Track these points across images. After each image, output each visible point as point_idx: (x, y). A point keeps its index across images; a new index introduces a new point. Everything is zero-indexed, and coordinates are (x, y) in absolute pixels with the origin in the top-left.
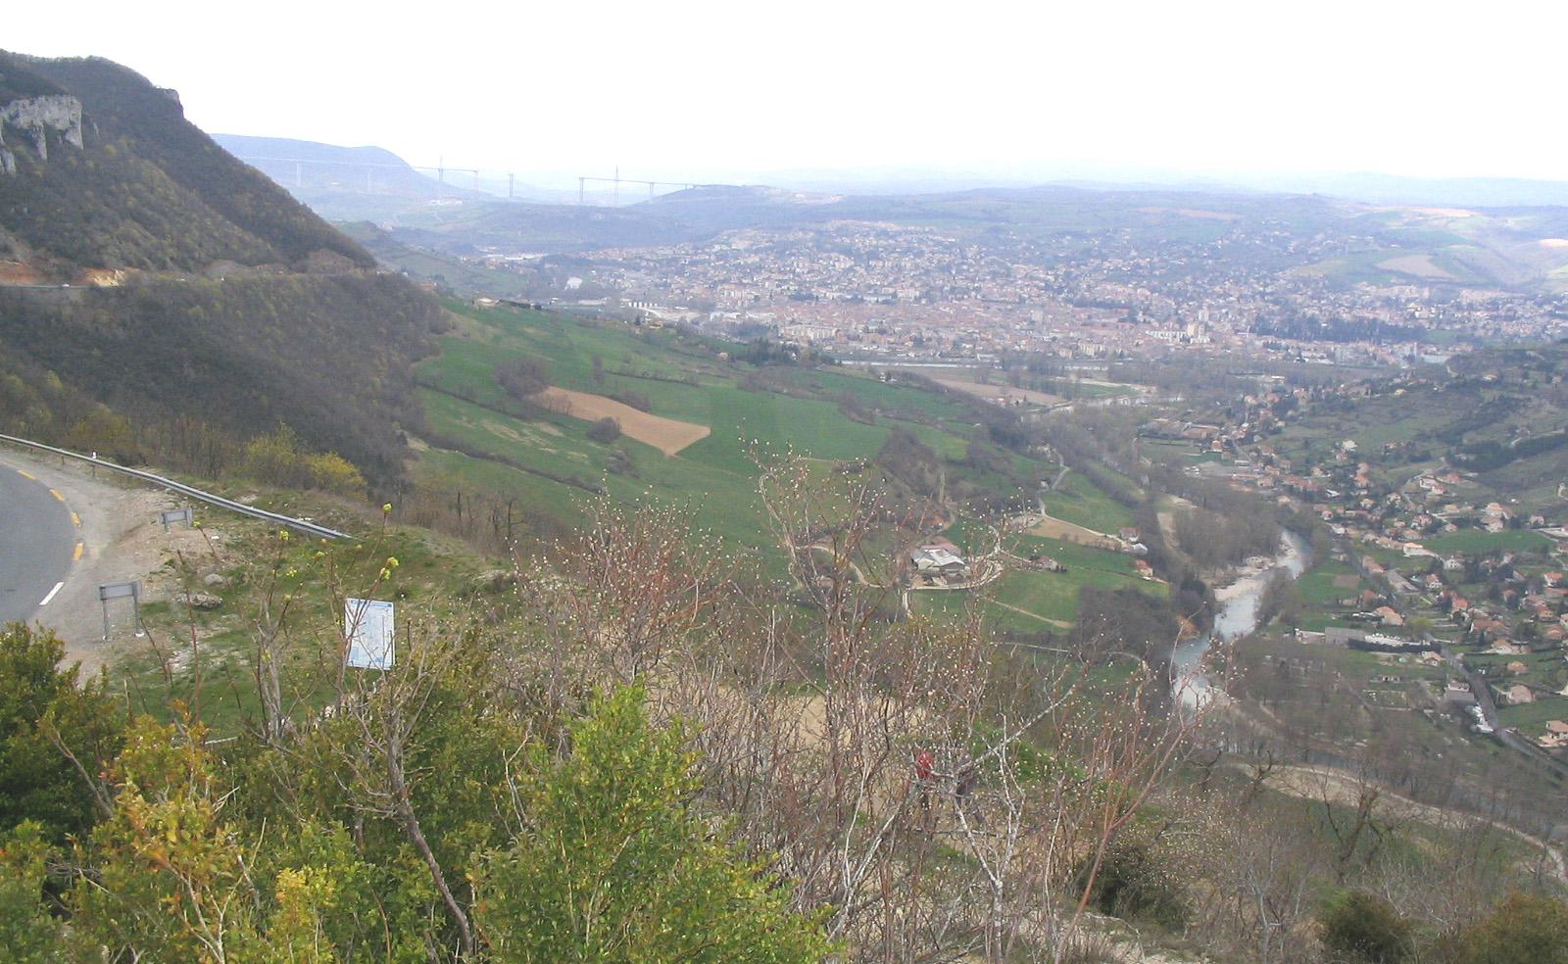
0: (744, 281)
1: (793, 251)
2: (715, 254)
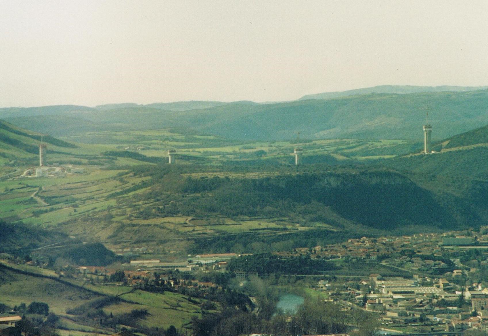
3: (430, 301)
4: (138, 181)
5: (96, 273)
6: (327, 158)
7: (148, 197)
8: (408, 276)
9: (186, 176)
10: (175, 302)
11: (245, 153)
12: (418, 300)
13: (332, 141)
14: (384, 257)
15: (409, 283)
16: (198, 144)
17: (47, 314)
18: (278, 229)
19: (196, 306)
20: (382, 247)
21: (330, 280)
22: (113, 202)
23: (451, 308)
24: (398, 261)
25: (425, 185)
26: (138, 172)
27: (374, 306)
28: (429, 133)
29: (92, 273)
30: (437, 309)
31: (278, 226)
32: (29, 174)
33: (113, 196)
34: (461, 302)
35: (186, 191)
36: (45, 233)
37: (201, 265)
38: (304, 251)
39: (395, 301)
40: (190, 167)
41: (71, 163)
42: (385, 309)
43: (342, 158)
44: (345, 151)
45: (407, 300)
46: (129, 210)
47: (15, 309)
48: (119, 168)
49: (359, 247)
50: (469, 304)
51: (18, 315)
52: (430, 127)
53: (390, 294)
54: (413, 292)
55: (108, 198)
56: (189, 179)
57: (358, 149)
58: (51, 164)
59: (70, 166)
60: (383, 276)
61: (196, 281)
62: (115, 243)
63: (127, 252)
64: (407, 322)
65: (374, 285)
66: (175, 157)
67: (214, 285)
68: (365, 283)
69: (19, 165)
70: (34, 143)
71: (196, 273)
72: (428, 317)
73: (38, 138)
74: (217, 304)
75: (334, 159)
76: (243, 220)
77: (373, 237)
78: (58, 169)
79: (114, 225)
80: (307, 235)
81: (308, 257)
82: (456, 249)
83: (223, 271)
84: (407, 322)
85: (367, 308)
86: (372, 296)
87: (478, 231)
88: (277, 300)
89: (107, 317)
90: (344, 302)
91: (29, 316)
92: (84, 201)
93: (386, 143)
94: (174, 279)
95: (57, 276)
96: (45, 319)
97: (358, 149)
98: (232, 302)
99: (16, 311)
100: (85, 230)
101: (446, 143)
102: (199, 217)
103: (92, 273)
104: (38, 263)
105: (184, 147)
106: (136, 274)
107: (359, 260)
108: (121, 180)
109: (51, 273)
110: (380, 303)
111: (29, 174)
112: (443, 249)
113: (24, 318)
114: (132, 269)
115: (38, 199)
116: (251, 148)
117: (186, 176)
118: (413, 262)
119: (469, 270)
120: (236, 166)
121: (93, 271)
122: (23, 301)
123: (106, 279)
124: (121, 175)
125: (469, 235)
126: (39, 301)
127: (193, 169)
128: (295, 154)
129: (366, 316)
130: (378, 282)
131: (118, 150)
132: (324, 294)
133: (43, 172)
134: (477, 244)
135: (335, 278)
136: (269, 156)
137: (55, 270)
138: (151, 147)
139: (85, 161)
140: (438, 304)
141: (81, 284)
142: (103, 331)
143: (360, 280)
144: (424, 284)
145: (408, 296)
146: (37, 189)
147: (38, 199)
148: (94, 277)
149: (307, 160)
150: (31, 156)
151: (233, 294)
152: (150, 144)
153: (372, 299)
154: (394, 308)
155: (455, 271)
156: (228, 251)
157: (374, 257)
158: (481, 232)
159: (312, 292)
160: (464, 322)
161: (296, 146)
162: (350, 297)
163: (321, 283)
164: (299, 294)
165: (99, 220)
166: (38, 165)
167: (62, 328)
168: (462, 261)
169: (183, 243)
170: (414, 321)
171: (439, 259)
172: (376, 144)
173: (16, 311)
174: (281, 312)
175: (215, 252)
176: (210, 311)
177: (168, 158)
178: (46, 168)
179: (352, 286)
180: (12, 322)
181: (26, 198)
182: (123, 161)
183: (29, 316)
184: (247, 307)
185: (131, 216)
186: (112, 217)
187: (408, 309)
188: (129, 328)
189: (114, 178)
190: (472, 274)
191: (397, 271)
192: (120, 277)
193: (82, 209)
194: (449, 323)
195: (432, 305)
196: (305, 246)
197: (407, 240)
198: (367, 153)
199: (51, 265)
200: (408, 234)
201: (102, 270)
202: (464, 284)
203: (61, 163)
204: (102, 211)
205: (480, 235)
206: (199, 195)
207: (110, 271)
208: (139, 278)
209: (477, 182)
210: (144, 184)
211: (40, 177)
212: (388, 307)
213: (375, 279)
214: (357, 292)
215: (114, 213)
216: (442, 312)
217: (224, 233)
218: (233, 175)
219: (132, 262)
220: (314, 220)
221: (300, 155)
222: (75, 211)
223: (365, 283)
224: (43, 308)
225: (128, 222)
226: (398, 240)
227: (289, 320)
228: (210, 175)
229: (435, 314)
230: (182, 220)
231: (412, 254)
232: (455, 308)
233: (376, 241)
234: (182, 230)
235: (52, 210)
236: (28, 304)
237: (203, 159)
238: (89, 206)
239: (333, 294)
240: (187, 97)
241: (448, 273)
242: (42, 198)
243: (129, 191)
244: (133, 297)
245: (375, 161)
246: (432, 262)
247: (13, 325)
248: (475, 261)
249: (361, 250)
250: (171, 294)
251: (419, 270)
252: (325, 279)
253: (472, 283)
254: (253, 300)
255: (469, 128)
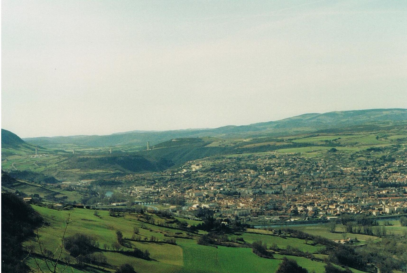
0: (200, 187)
1: (226, 170)
2: (184, 174)
3: (150, 192)
4: (64, 158)
5: (52, 186)
6: (120, 151)
7: (67, 163)
8: (143, 185)
9: (78, 157)
10: (75, 194)
11: (95, 150)
12: (146, 192)
13: (121, 146)
14: (137, 180)
15: (143, 187)
16: (82, 148)
17: (39, 197)
18: (105, 172)
19: (82, 195)
20: (136, 177)
21: (120, 187)
22: (57, 165)
23: (155, 194)
24: (140, 181)
25: (148, 159)
26: (64, 156)
27: (133, 194)
28: (149, 144)
29: (51, 186)
30: (151, 194)
31: (106, 172)
32: (33, 157)
33: (57, 163)
34: (158, 192)
35: (78, 162)
36: (38, 174)
37: (83, 183)
38: (113, 179)
39: (140, 193)
40: (79, 154)
41: (45, 153)
42: (137, 195)
43: (124, 151)
44: (125, 149)
45: (143, 192)
46: (61, 167)
47: (30, 196)
48: (58, 155)
49: (129, 177)
50: (160, 193)
51: (30, 197)
52: (149, 142)
53: (138, 191)
54: (145, 190)
55: (55, 164)
56: (79, 158)
57: (128, 149)
58: (39, 154)
59: (45, 155)
60: (136, 185)
61: (82, 188)
62: (58, 177)
63: (61, 179)
64: (143, 199)
65: (133, 188)
66: (75, 151)
67: (87, 189)
68: (131, 188)
69: (30, 154)
70: (34, 148)
71: (82, 185)
72: (149, 197)
73: (35, 146)
74: (87, 194)
75: (121, 152)
76: (96, 170)
77: (133, 175)
78: (41, 155)
79: (57, 172)
80: (114, 174)
81: (114, 181)
82: (157, 177)
83: (90, 185)
84: (143, 199)
85: (132, 195)
86: (133, 191)
87: (163, 172)
88: (106, 193)
89: (56, 198)
90: (125, 193)
91: (34, 198)
92: (49, 165)
93: (137, 147)
94: (75, 187)
95: (41, 186)
96: (38, 199)
97: (128, 149)
98: (92, 194)
99: (30, 196)
100: (49, 173)
101: (153, 147)
102: (82, 169)
103: (51, 186)
104: (36, 183)
105: (78, 149)
106: (64, 186)
107: (129, 181)
108: (59, 159)
109: (40, 186)
110: (135, 193)
111: (33, 157)
112: (153, 177)
113: (32, 198)
114: (63, 184)
115: (35, 164)
116: (97, 149)
117: (78, 157)
118: (145, 181)
119: (160, 183)
120: (93, 154)
121: (51, 185)
122: (32, 194)
123: (55, 188)
124: (59, 157)
125: (160, 173)
126: (37, 193)
127: (79, 155)
128: (110, 150)
129: (132, 197)
130: (135, 187)
131: (58, 150)
132: (119, 191)
133: (37, 156)
134: (162, 176)
135: (122, 186)
136: (102, 151)
137: (41, 185)
138: (68, 148)
139: (48, 153)
140: (152, 193)
141: (48, 189)
142: (55, 202)
143: (130, 187)
144: (148, 188)
145: (143, 191)
146: (35, 161)
147: (35, 164)
148: (52, 187)
149: (113, 152)
150: (33, 152)
151: (93, 192)
152: (68, 148)
153: (133, 192)
154: (139, 195)
155: (156, 184)
156: (91, 179)
157: (133, 180)
158: (164, 172)
159: (116, 191)
160: (159, 198)
161: (110, 148)
162: (127, 192)
163: (118, 188)
164: (112, 191)
165: (53, 170)
166: (35, 154)
167: (43, 201)
168: (158, 181)
169: (78, 177)
170: (145, 198)
171: (152, 180)
172: (134, 147)
173: (30, 196)
174: (106, 196)
175: (87, 179)
176: (86, 197)
177: (73, 152)
178: (38, 155)
179: (127, 188)
180: (29, 199)
181: (32, 164)
182: (60, 153)
183: (34, 198)
184: (97, 195)
185: (62, 169)
186: (57, 169)
187: (143, 195)
188: (62, 201)
189: (57, 158)
190: (161, 184)
191: (140, 184)
192: (59, 187)
193: (48, 167)
194: (155, 198)
195: (150, 194)
196: (114, 177)
197: (143, 175)
198: (131, 150)
199: (39, 183)
200: (144, 173)
201: (54, 185)
202: (159, 187)
203: (42, 154)
204: (54, 168)
205: (163, 173)
206: (82, 163)
207: (56, 185)
208: (65, 187)
209: (162, 158)
210: (66, 160)
211: (36, 158)
212: (137, 194)
213: (134, 186)
214: (129, 190)
215: (57, 168)
216: (152, 195)
217: (90, 174)
218: (92, 157)
219: (63, 182)
220: (116, 170)
221: (112, 151)
222: (46, 168)
223: (131, 188)
224: (37, 196)
225: (61, 171)
226: (140, 175)
227: (109, 199)
228: (85, 157)
229: (151, 196)
230: (77, 170)
231: (144, 179)
232: (156, 194)
233: (134, 176)
234: (77, 173)
235: (40, 167)
236: (33, 194)
237: (83, 152)
238: (50, 166)
239: (122, 191)
240: (78, 134)
241: (154, 184)
242: (37, 164)
243: (62, 161)
244: (63, 192)
245: (134, 152)
246: (150, 181)
247: (30, 200)
248: (162, 181)
249: (130, 178)
250: (74, 192)
251: (146, 184)
252: (119, 187)
253: (161, 187)
254: (98, 193)
255: (160, 142)
